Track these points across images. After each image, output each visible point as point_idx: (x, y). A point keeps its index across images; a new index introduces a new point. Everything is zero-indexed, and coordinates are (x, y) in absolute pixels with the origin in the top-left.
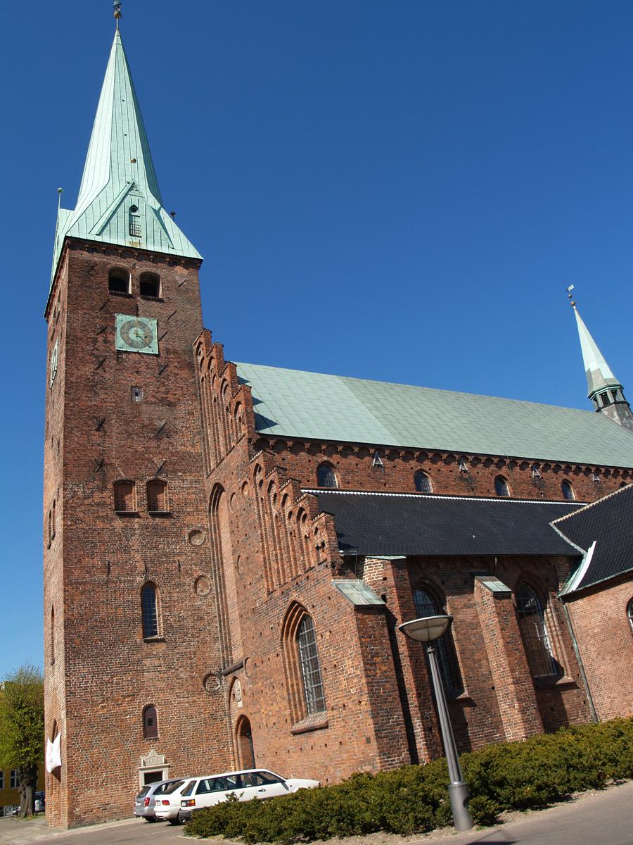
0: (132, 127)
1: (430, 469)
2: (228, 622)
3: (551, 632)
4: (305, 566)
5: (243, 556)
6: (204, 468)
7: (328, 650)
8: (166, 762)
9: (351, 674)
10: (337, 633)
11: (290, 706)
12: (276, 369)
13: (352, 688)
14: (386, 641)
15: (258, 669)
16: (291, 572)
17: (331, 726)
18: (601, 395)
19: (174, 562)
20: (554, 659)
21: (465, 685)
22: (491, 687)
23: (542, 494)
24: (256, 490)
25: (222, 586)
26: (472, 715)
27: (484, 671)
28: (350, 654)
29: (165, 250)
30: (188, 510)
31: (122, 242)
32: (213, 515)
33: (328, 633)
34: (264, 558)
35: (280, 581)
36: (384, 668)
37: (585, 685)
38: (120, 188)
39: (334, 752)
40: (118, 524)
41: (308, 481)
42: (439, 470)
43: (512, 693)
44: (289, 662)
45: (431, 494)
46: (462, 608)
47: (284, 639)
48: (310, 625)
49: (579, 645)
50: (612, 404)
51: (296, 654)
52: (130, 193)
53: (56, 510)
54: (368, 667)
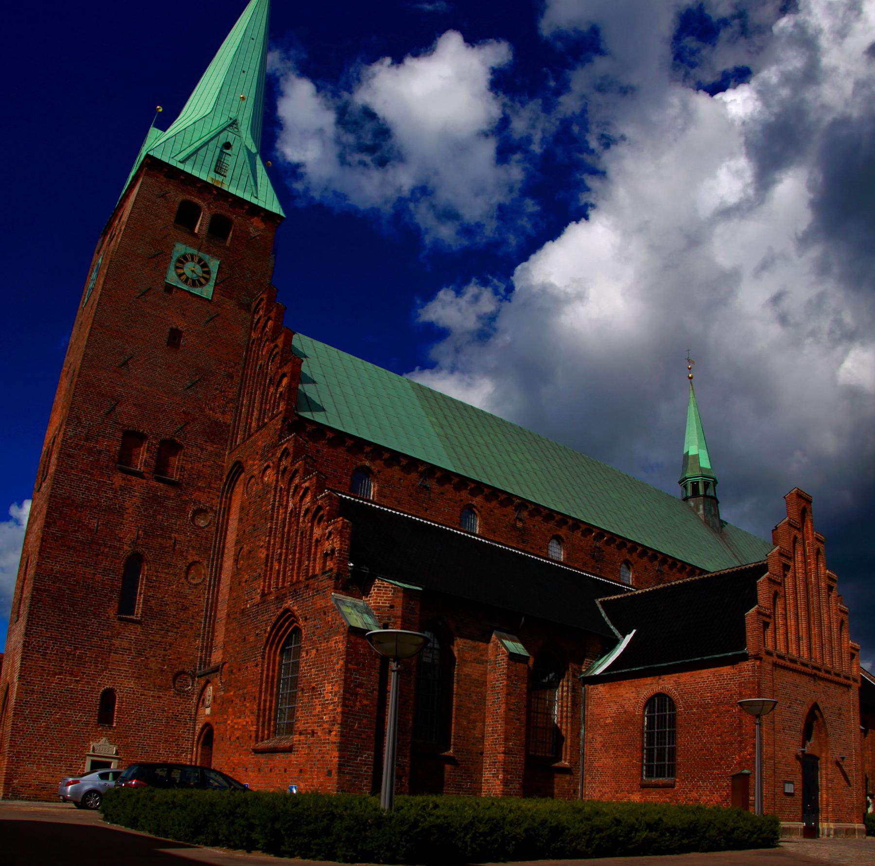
0: (253, 66)
1: (482, 507)
2: (214, 620)
3: (562, 711)
4: (308, 572)
5: (246, 548)
6: (229, 443)
7: (311, 669)
8: (117, 753)
9: (327, 700)
10: (324, 652)
11: (258, 722)
12: (340, 351)
13: (325, 715)
14: (375, 673)
15: (233, 676)
16: (292, 576)
17: (294, 751)
18: (692, 483)
19: (170, 538)
20: (556, 725)
21: (452, 743)
22: (479, 751)
23: (598, 568)
24: (277, 477)
25: (218, 579)
26: (451, 775)
27: (477, 733)
28: (332, 678)
29: (247, 197)
30: (199, 484)
31: (203, 176)
32: (226, 498)
33: (314, 651)
34: (267, 555)
35: (277, 584)
36: (365, 702)
37: (580, 774)
38: (221, 121)
39: (292, 778)
40: (118, 479)
41: (340, 483)
42: (492, 511)
43: (499, 762)
44: (268, 675)
45: (475, 535)
46: (471, 661)
47: (267, 649)
48: (299, 639)
49: (586, 732)
50: (701, 496)
51: (277, 668)
52: (228, 129)
53: (54, 448)
54: (348, 696)
